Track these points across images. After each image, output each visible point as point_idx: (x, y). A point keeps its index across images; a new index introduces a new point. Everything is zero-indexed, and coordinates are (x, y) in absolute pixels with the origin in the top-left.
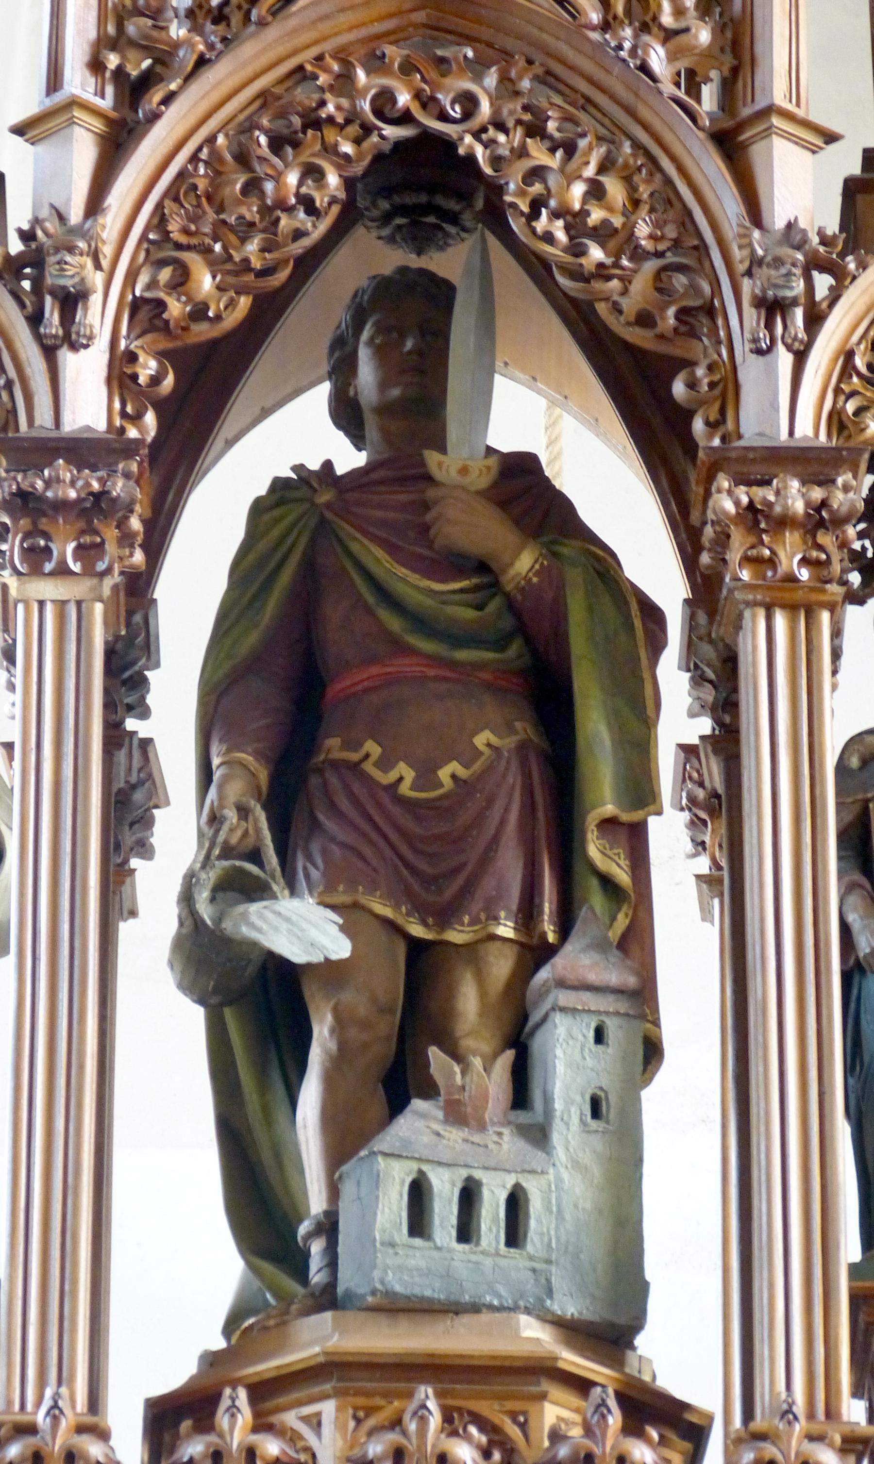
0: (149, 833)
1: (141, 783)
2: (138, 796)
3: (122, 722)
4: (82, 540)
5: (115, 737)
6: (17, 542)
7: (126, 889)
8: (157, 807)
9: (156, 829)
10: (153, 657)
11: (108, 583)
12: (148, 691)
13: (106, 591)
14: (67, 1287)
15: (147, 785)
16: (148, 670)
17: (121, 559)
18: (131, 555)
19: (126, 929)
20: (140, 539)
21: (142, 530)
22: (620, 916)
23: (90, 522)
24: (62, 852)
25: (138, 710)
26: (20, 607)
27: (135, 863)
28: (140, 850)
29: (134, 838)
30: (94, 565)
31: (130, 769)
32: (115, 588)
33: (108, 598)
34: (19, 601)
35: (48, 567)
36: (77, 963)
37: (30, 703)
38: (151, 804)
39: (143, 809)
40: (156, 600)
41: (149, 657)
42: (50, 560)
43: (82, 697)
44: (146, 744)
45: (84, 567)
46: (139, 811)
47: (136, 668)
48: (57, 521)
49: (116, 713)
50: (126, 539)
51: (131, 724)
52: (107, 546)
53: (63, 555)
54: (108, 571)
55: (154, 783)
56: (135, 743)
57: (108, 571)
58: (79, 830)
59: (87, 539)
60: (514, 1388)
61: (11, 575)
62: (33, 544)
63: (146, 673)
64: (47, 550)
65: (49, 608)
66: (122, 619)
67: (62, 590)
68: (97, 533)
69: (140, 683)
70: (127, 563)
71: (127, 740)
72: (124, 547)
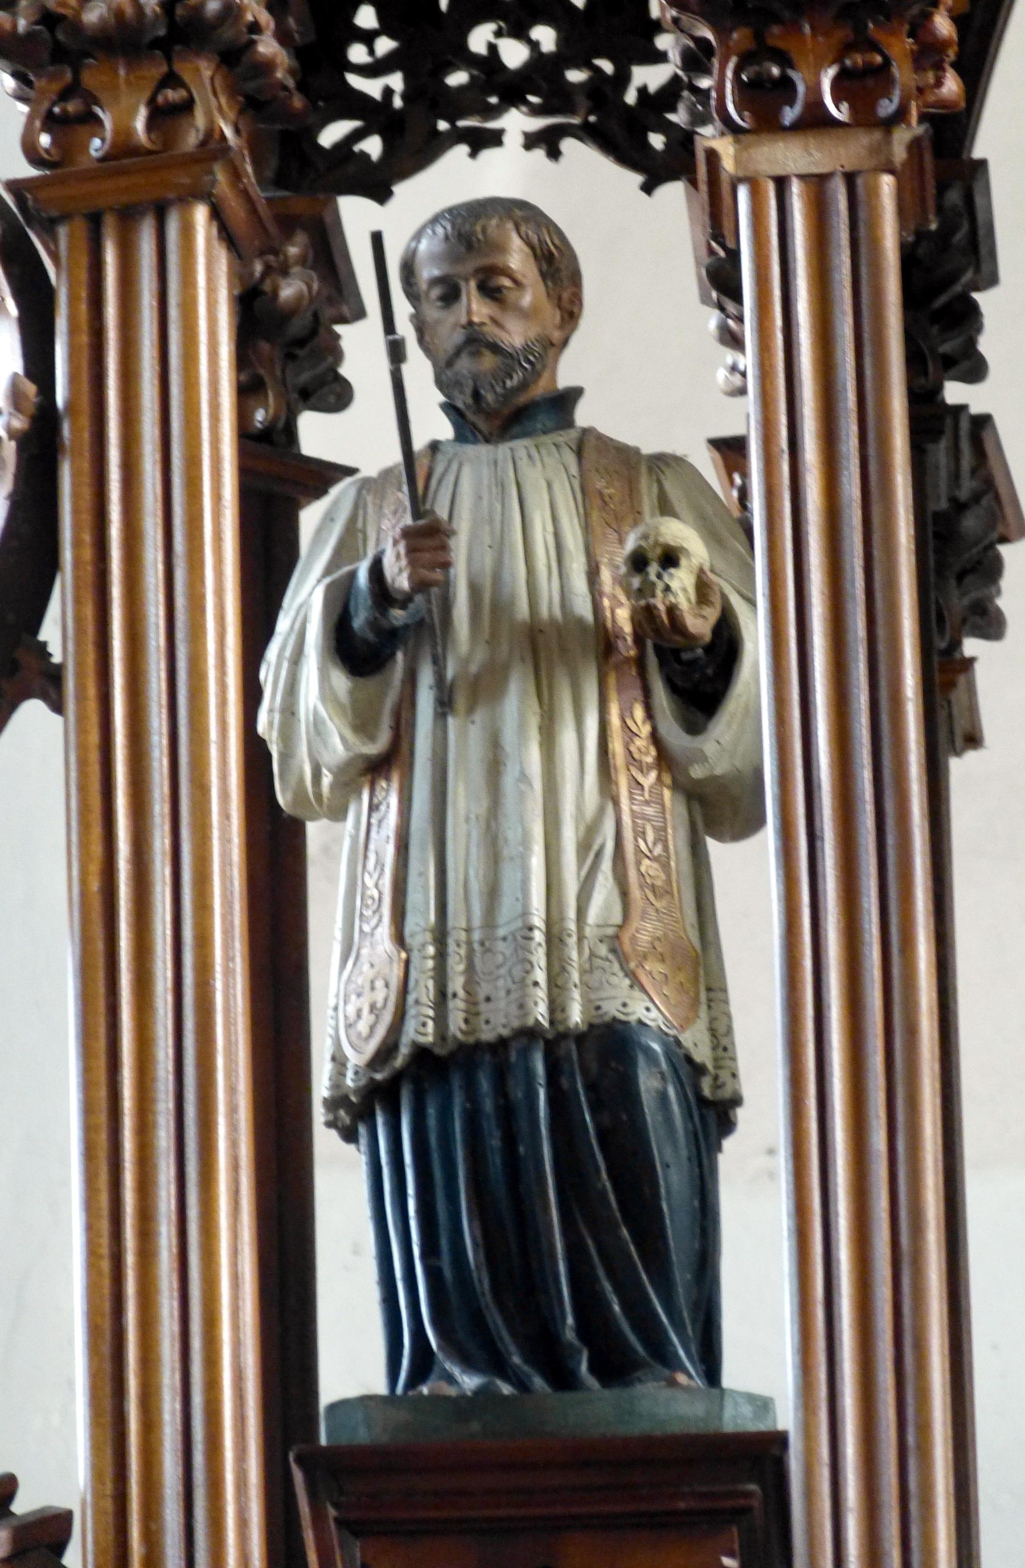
0: (993, 590)
1: (976, 498)
2: (970, 523)
3: (939, 389)
4: (848, 62)
5: (930, 418)
6: (729, 74)
7: (958, 696)
8: (1004, 540)
9: (1007, 582)
10: (985, 268)
11: (901, 138)
12: (979, 328)
13: (899, 153)
14: (911, 1439)
15: (984, 502)
16: (978, 289)
17: (921, 90)
18: (939, 83)
19: (960, 768)
20: (952, 54)
21: (955, 37)
22: (455, 335)
23: (860, 29)
24: (850, 637)
25: (965, 365)
26: (743, 194)
27: (971, 646)
28: (978, 619)
29: (966, 601)
30: (873, 106)
31: (955, 477)
32: (915, 146)
33: (904, 165)
34: (741, 180)
35: (789, 115)
36: (891, 840)
37: (772, 366)
38: (995, 536)
39: (980, 547)
40: (983, 164)
41: (978, 269)
42: (791, 103)
43: (867, 349)
44: (983, 422)
45: (853, 108)
46: (975, 550)
47: (958, 288)
48: (799, 30)
49: (926, 373)
50: (928, 54)
51: (954, 392)
52: (895, 71)
53: (815, 90)
54: (900, 116)
55: (997, 498)
56: (965, 426)
57: (900, 116)
58: (879, 595)
59: (856, 60)
60: (685, 1314)
61: (722, 134)
62: (758, 74)
63: (976, 296)
64: (786, 85)
65: (796, 188)
66: (931, 203)
67: (817, 155)
68: (874, 47)
69: (966, 318)
70: (931, 98)
71: (949, 421)
72: (925, 70)
